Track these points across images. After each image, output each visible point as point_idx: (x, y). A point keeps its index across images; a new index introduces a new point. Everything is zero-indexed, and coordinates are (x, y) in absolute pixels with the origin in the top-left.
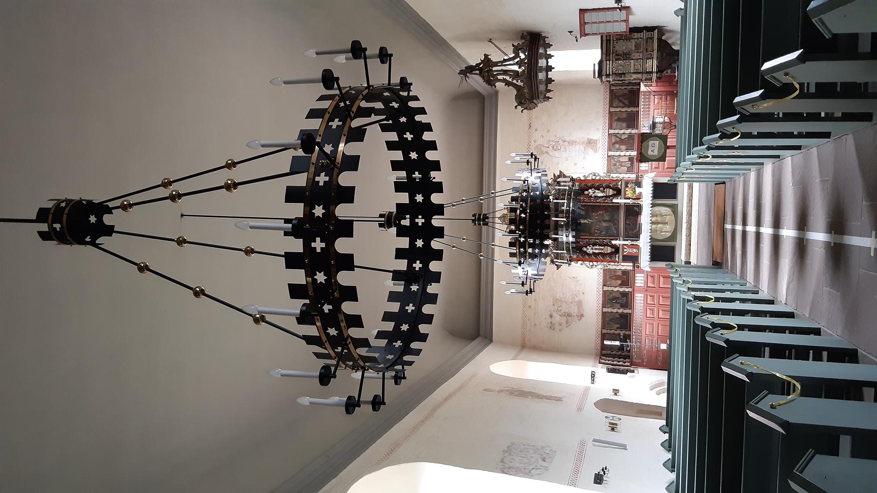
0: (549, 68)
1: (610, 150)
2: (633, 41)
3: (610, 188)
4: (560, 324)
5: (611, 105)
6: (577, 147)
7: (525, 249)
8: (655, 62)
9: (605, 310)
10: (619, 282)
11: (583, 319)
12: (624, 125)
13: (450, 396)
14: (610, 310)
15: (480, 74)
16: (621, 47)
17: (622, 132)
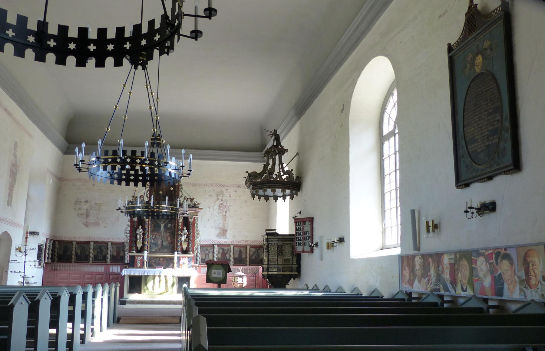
0: (276, 198)
1: (219, 246)
2: (291, 257)
3: (188, 245)
4: (80, 209)
5: (251, 246)
6: (221, 222)
7: (111, 163)
8: (276, 273)
9: (92, 244)
10: (115, 254)
11: (84, 227)
12: (237, 256)
13: (9, 114)
14: (92, 247)
15: (273, 146)
16: (287, 249)
17: (232, 254)
